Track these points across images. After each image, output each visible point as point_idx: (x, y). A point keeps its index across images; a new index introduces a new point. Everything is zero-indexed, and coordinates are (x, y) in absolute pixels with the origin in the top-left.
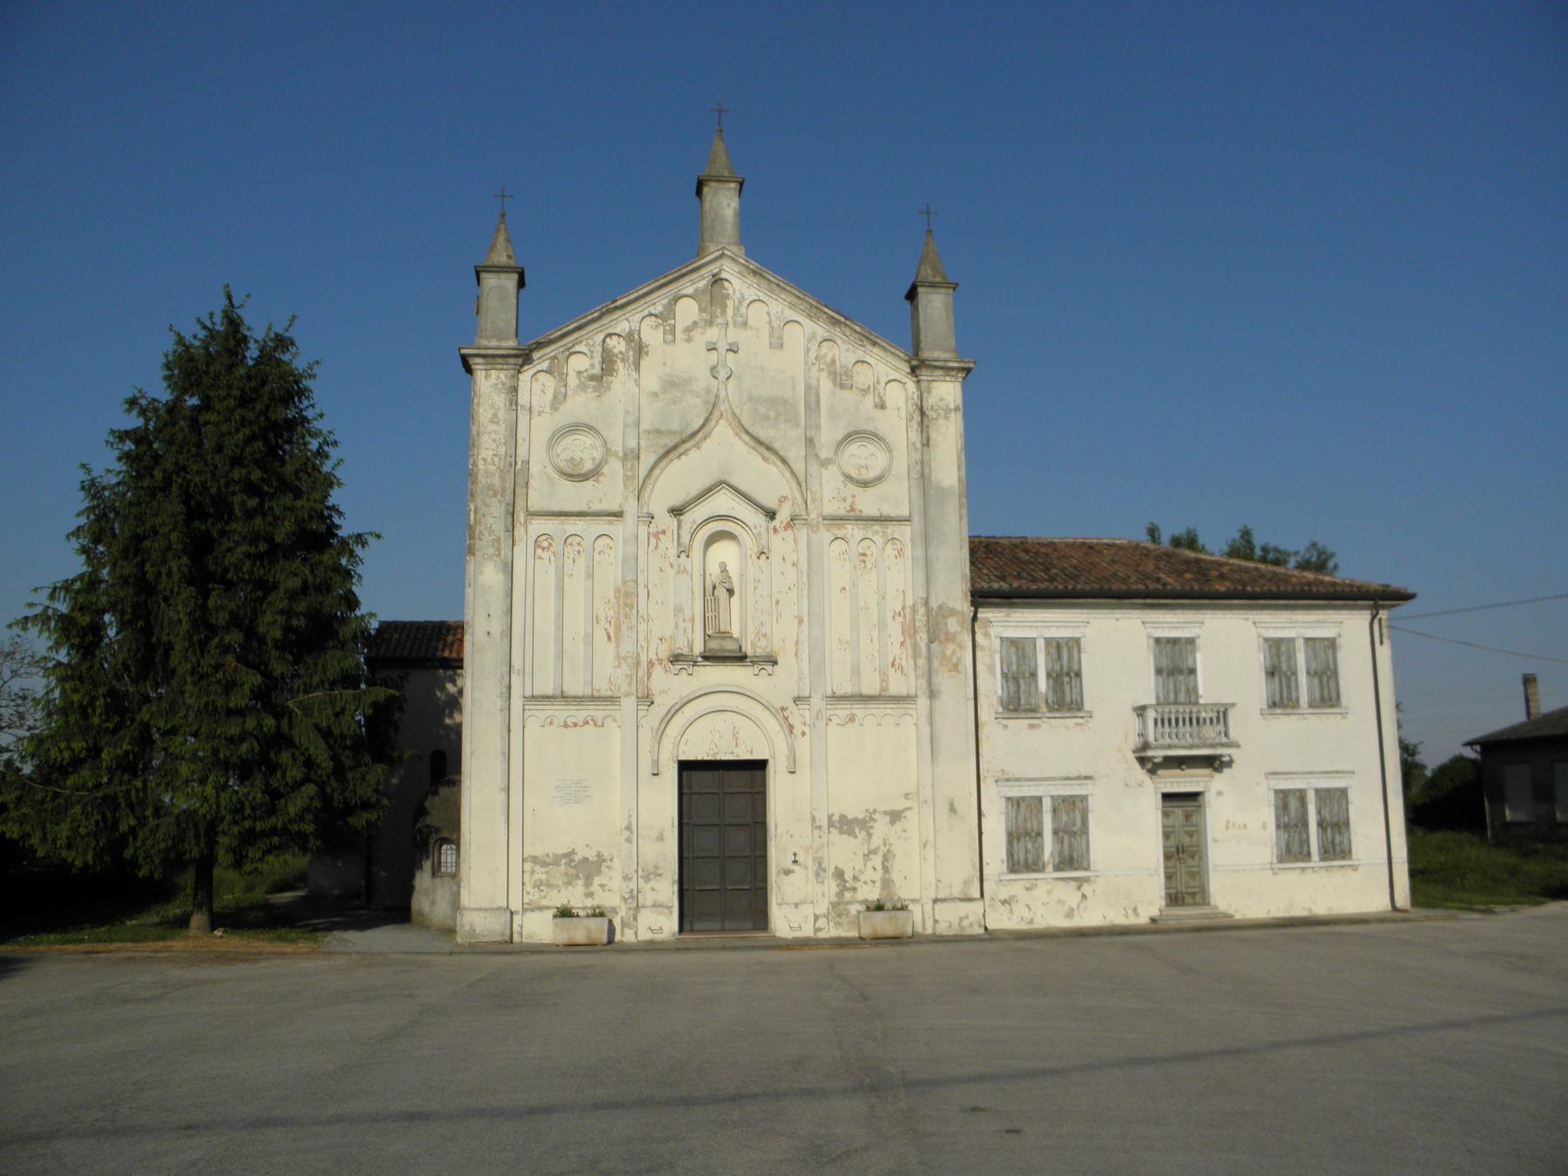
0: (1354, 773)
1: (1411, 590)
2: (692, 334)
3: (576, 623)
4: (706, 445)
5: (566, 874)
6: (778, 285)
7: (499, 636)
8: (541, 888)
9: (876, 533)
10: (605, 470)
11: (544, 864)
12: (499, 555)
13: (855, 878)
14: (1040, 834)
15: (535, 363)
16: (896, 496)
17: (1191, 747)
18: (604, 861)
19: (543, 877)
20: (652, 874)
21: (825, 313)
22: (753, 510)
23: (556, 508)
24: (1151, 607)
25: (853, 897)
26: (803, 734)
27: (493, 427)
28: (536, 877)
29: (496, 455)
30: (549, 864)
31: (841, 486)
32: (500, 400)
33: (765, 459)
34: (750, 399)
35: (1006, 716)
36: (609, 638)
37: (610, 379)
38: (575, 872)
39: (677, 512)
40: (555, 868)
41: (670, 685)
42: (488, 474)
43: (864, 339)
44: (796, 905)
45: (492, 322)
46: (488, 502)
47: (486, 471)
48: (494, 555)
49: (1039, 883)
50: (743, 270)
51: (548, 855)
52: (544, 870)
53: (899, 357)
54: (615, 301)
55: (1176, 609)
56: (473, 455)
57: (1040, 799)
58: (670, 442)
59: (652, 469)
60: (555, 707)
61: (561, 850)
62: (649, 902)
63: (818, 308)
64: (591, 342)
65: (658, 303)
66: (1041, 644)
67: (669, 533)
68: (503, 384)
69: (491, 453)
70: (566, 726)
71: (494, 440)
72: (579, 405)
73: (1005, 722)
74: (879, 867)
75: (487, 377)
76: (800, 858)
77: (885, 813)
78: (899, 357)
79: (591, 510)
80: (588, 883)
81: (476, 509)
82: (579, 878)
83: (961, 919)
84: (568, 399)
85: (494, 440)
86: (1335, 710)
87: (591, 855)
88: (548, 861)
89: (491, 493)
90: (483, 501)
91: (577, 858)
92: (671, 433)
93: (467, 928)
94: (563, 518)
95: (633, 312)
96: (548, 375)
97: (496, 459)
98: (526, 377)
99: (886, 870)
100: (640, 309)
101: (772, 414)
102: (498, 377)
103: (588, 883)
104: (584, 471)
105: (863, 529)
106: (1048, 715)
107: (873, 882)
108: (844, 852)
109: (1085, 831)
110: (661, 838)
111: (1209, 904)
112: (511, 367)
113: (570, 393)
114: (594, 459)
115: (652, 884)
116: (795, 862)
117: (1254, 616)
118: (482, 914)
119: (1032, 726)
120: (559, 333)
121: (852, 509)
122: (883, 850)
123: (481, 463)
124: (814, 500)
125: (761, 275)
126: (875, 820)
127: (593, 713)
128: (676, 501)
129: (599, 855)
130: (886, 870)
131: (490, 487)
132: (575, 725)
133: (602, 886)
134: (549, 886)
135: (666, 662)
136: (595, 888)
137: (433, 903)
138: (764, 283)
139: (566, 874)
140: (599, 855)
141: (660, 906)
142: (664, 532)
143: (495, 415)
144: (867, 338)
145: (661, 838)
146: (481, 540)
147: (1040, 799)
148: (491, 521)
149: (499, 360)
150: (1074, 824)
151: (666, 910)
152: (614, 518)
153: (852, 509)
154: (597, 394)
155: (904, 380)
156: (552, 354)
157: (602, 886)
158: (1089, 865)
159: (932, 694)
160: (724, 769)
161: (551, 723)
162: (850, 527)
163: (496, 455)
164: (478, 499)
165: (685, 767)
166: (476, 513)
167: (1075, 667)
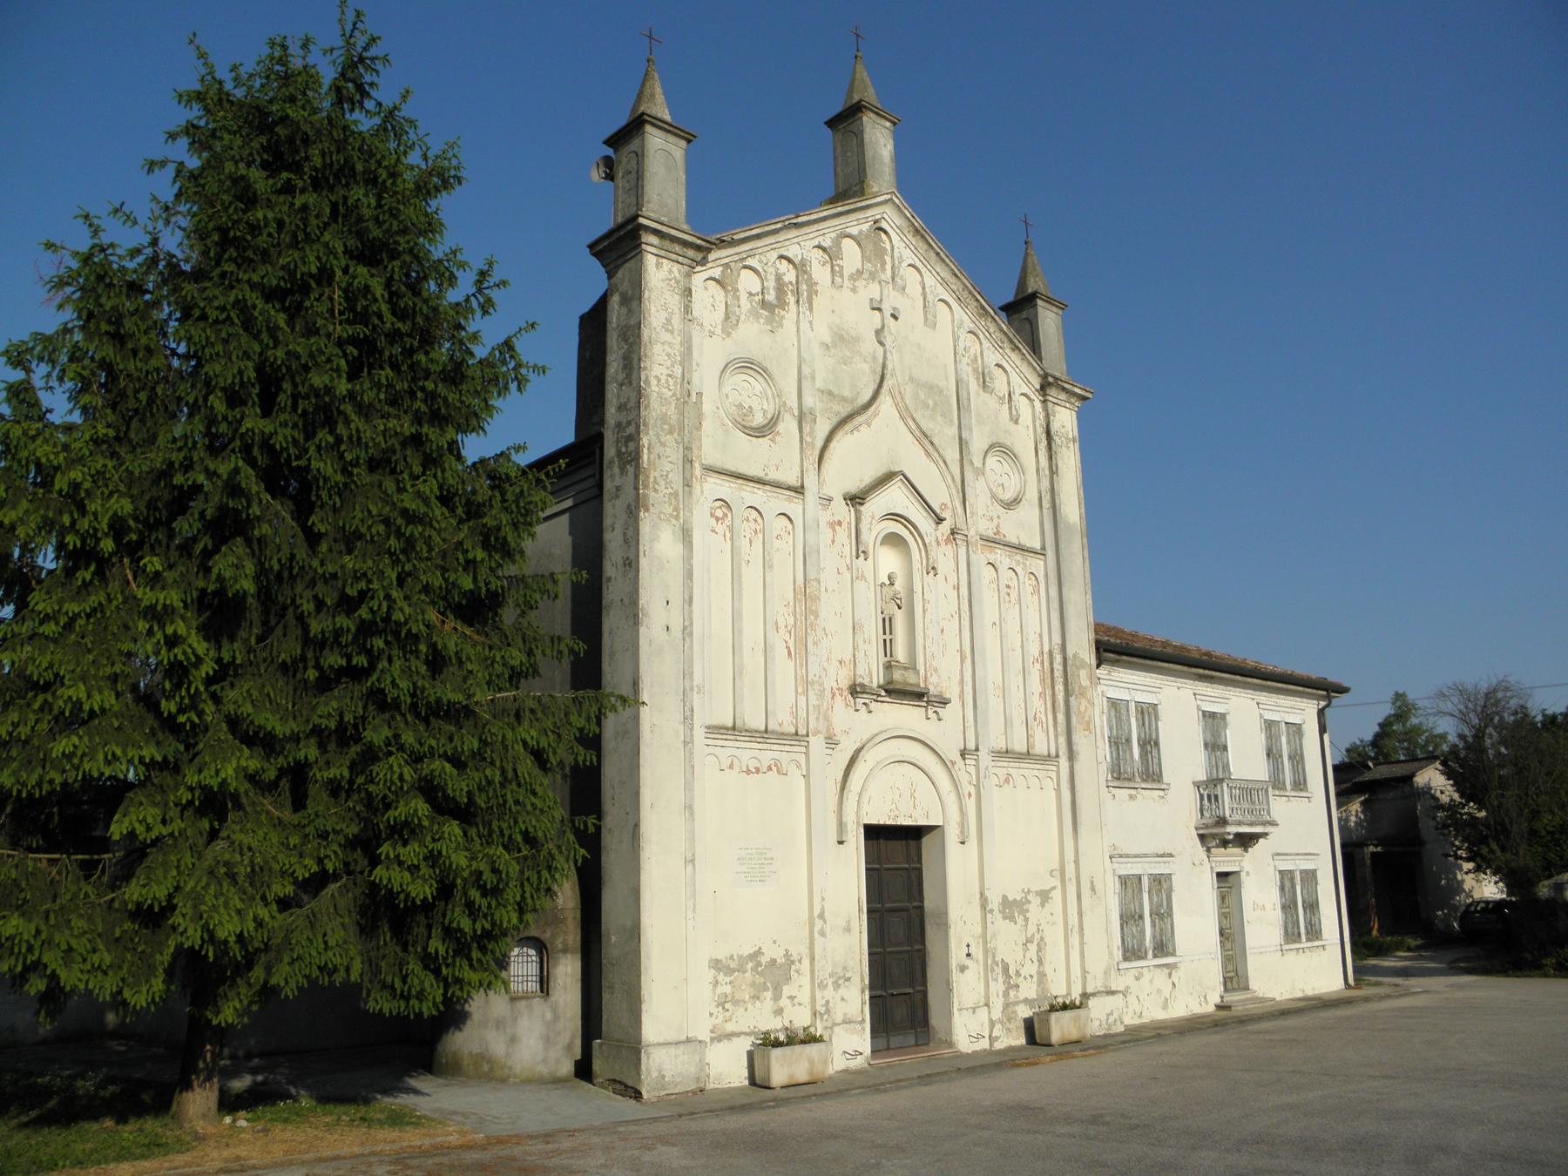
0: (1171, 855)
1: (1346, 684)
2: (857, 284)
3: (753, 631)
4: (875, 423)
5: (753, 984)
6: (938, 254)
7: (680, 635)
8: (727, 1006)
9: (1018, 563)
10: (781, 427)
11: (729, 971)
12: (677, 518)
13: (1018, 974)
14: (1141, 917)
15: (709, 265)
16: (1025, 525)
17: (1251, 824)
18: (793, 962)
19: (728, 989)
20: (840, 980)
21: (977, 300)
22: (925, 514)
23: (732, 467)
24: (1201, 678)
25: (1016, 996)
26: (970, 795)
27: (666, 337)
28: (720, 990)
29: (670, 376)
30: (734, 971)
31: (989, 503)
32: (675, 301)
33: (928, 454)
34: (911, 379)
35: (1115, 784)
36: (789, 653)
37: (782, 313)
38: (762, 980)
39: (856, 500)
40: (741, 975)
41: (856, 723)
42: (664, 401)
43: (1006, 340)
44: (974, 1010)
45: (659, 195)
46: (663, 439)
47: (660, 395)
48: (671, 515)
49: (1145, 971)
50: (904, 224)
51: (732, 957)
52: (728, 979)
53: (1035, 369)
54: (797, 217)
55: (1227, 685)
56: (645, 368)
57: (1139, 878)
58: (845, 410)
59: (828, 440)
60: (737, 744)
61: (748, 950)
62: (839, 1019)
63: (970, 293)
64: (763, 258)
65: (826, 234)
66: (1132, 706)
67: (845, 525)
68: (677, 282)
69: (666, 372)
70: (748, 772)
71: (668, 355)
72: (751, 335)
73: (1114, 791)
74: (1035, 959)
75: (658, 265)
76: (973, 950)
77: (1037, 893)
78: (1035, 369)
79: (767, 478)
80: (777, 997)
81: (650, 444)
82: (766, 989)
83: (1108, 1015)
84: (740, 325)
85: (668, 355)
86: (1302, 794)
87: (777, 954)
88: (733, 965)
89: (666, 427)
90: (658, 435)
91: (764, 959)
92: (844, 399)
93: (655, 1074)
94: (740, 481)
95: (805, 237)
96: (718, 287)
97: (671, 382)
98: (698, 279)
99: (1040, 961)
100: (811, 236)
101: (931, 403)
102: (670, 271)
103: (777, 997)
104: (754, 424)
105: (1010, 557)
106: (1143, 786)
107: (1031, 976)
108: (1007, 940)
109: (1170, 915)
110: (848, 930)
111: (1247, 988)
112: (686, 261)
113: (742, 317)
114: (765, 412)
115: (842, 991)
116: (968, 955)
117: (1264, 697)
118: (672, 1050)
119: (1132, 797)
120: (742, 235)
121: (998, 533)
122: (1037, 936)
123: (653, 382)
124: (972, 513)
125: (923, 236)
126: (1029, 902)
127: (777, 755)
128: (854, 486)
129: (787, 955)
130: (1040, 961)
131: (664, 418)
132: (758, 770)
133: (792, 998)
134: (736, 1003)
135: (846, 693)
136: (784, 1002)
137: (513, 1040)
138: (922, 246)
139: (753, 984)
140: (787, 955)
141: (850, 1022)
142: (840, 523)
143: (668, 320)
144: (1011, 341)
145: (848, 930)
146: (656, 491)
147: (1139, 878)
148: (668, 467)
149: (677, 248)
150: (1161, 906)
151: (858, 1027)
152: (792, 494)
153: (998, 533)
154: (769, 328)
155: (1033, 397)
156: (726, 260)
157: (792, 998)
158: (1174, 950)
159: (1072, 756)
160: (887, 839)
161: (731, 767)
162: (999, 551)
163: (670, 376)
164: (651, 432)
165: (874, 833)
166: (649, 452)
167: (1154, 736)
